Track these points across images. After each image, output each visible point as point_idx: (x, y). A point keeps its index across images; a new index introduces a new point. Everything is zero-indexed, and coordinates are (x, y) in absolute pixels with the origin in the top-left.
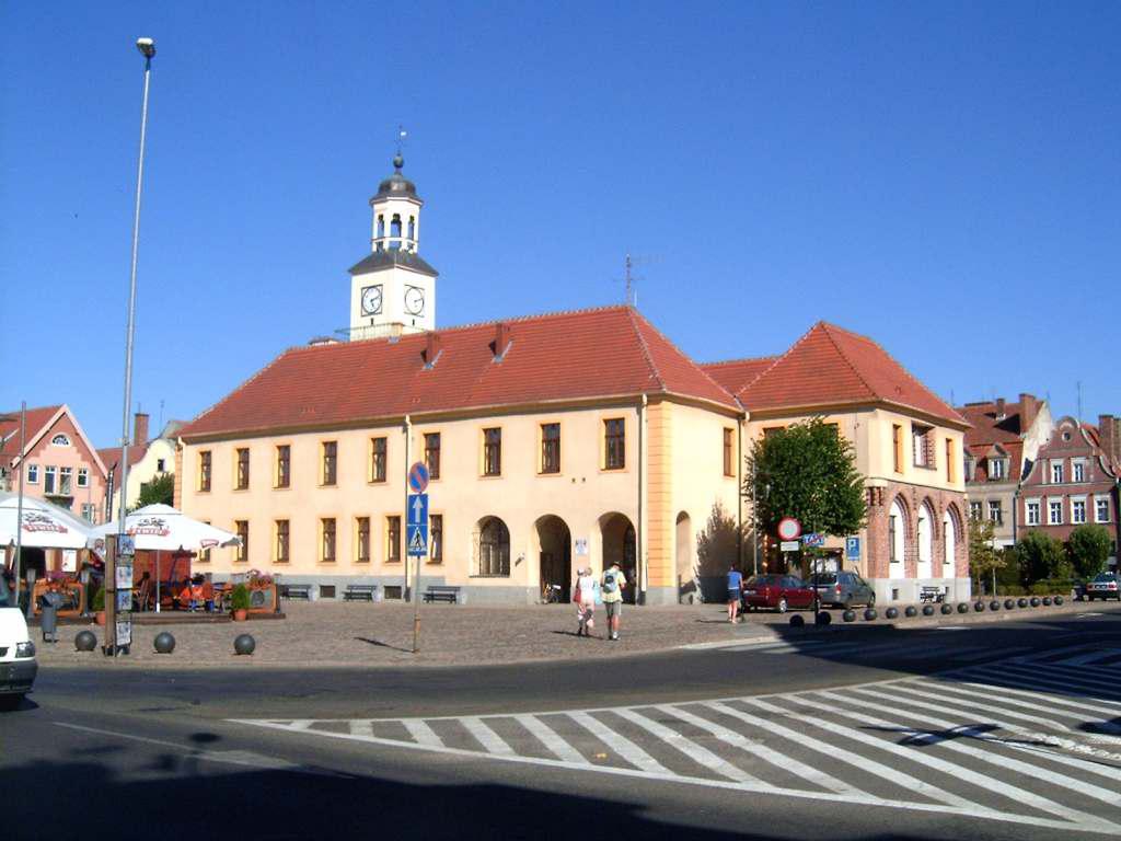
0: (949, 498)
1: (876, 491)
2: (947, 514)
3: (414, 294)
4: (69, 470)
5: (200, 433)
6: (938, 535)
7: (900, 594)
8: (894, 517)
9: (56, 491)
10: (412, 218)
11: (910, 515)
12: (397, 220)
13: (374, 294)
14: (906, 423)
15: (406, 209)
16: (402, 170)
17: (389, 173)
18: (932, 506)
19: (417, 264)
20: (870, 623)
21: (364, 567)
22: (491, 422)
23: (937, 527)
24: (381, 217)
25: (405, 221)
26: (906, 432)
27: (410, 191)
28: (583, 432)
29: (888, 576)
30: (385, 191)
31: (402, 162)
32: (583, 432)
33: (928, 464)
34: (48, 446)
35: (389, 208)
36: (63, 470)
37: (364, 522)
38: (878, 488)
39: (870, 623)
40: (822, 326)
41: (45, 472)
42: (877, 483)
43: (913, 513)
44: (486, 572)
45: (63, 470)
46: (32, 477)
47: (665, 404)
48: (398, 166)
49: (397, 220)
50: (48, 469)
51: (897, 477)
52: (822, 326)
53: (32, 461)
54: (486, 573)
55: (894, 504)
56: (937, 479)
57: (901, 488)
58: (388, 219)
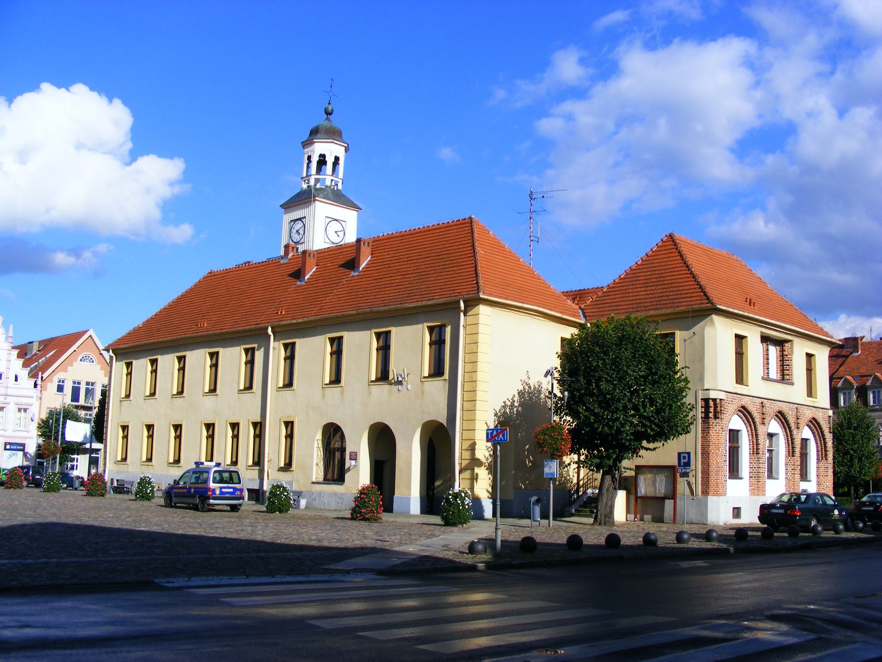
0: (808, 414)
1: (711, 403)
2: (806, 429)
3: (335, 226)
4: (93, 384)
5: (126, 350)
6: (793, 452)
7: (743, 512)
8: (807, 440)
9: (82, 402)
10: (337, 159)
11: (756, 430)
12: (322, 161)
13: (299, 225)
14: (753, 335)
15: (331, 149)
16: (331, 117)
17: (320, 120)
18: (787, 422)
19: (338, 198)
20: (681, 545)
21: (122, 467)
22: (740, 389)
23: (793, 443)
24: (309, 158)
25: (330, 161)
26: (754, 348)
27: (334, 134)
28: (411, 343)
29: (724, 494)
30: (315, 132)
31: (333, 111)
32: (411, 343)
33: (785, 377)
34: (75, 363)
35: (320, 147)
36: (88, 384)
37: (235, 426)
38: (714, 400)
39: (681, 545)
40: (671, 236)
41: (72, 384)
42: (713, 395)
43: (761, 430)
44: (327, 480)
45: (88, 384)
46: (60, 389)
47: (483, 309)
48: (328, 113)
49: (322, 161)
50: (74, 383)
51: (740, 389)
52: (671, 236)
53: (60, 375)
54: (327, 480)
55: (773, 421)
56: (796, 392)
57: (746, 401)
58: (315, 159)
